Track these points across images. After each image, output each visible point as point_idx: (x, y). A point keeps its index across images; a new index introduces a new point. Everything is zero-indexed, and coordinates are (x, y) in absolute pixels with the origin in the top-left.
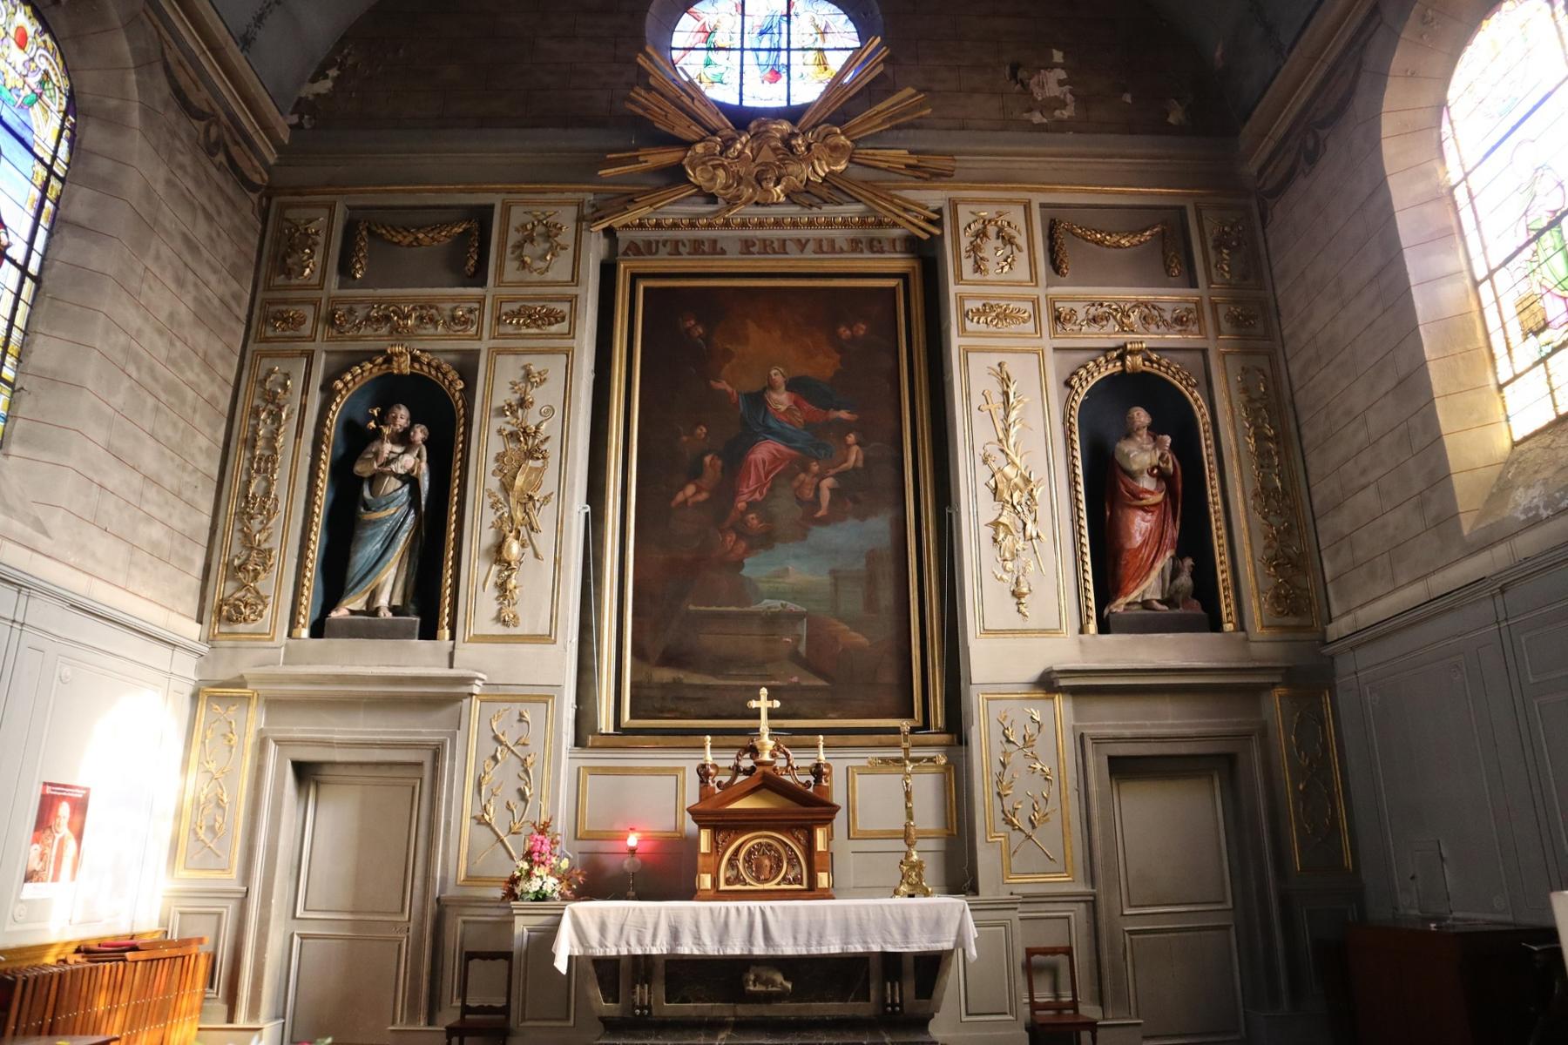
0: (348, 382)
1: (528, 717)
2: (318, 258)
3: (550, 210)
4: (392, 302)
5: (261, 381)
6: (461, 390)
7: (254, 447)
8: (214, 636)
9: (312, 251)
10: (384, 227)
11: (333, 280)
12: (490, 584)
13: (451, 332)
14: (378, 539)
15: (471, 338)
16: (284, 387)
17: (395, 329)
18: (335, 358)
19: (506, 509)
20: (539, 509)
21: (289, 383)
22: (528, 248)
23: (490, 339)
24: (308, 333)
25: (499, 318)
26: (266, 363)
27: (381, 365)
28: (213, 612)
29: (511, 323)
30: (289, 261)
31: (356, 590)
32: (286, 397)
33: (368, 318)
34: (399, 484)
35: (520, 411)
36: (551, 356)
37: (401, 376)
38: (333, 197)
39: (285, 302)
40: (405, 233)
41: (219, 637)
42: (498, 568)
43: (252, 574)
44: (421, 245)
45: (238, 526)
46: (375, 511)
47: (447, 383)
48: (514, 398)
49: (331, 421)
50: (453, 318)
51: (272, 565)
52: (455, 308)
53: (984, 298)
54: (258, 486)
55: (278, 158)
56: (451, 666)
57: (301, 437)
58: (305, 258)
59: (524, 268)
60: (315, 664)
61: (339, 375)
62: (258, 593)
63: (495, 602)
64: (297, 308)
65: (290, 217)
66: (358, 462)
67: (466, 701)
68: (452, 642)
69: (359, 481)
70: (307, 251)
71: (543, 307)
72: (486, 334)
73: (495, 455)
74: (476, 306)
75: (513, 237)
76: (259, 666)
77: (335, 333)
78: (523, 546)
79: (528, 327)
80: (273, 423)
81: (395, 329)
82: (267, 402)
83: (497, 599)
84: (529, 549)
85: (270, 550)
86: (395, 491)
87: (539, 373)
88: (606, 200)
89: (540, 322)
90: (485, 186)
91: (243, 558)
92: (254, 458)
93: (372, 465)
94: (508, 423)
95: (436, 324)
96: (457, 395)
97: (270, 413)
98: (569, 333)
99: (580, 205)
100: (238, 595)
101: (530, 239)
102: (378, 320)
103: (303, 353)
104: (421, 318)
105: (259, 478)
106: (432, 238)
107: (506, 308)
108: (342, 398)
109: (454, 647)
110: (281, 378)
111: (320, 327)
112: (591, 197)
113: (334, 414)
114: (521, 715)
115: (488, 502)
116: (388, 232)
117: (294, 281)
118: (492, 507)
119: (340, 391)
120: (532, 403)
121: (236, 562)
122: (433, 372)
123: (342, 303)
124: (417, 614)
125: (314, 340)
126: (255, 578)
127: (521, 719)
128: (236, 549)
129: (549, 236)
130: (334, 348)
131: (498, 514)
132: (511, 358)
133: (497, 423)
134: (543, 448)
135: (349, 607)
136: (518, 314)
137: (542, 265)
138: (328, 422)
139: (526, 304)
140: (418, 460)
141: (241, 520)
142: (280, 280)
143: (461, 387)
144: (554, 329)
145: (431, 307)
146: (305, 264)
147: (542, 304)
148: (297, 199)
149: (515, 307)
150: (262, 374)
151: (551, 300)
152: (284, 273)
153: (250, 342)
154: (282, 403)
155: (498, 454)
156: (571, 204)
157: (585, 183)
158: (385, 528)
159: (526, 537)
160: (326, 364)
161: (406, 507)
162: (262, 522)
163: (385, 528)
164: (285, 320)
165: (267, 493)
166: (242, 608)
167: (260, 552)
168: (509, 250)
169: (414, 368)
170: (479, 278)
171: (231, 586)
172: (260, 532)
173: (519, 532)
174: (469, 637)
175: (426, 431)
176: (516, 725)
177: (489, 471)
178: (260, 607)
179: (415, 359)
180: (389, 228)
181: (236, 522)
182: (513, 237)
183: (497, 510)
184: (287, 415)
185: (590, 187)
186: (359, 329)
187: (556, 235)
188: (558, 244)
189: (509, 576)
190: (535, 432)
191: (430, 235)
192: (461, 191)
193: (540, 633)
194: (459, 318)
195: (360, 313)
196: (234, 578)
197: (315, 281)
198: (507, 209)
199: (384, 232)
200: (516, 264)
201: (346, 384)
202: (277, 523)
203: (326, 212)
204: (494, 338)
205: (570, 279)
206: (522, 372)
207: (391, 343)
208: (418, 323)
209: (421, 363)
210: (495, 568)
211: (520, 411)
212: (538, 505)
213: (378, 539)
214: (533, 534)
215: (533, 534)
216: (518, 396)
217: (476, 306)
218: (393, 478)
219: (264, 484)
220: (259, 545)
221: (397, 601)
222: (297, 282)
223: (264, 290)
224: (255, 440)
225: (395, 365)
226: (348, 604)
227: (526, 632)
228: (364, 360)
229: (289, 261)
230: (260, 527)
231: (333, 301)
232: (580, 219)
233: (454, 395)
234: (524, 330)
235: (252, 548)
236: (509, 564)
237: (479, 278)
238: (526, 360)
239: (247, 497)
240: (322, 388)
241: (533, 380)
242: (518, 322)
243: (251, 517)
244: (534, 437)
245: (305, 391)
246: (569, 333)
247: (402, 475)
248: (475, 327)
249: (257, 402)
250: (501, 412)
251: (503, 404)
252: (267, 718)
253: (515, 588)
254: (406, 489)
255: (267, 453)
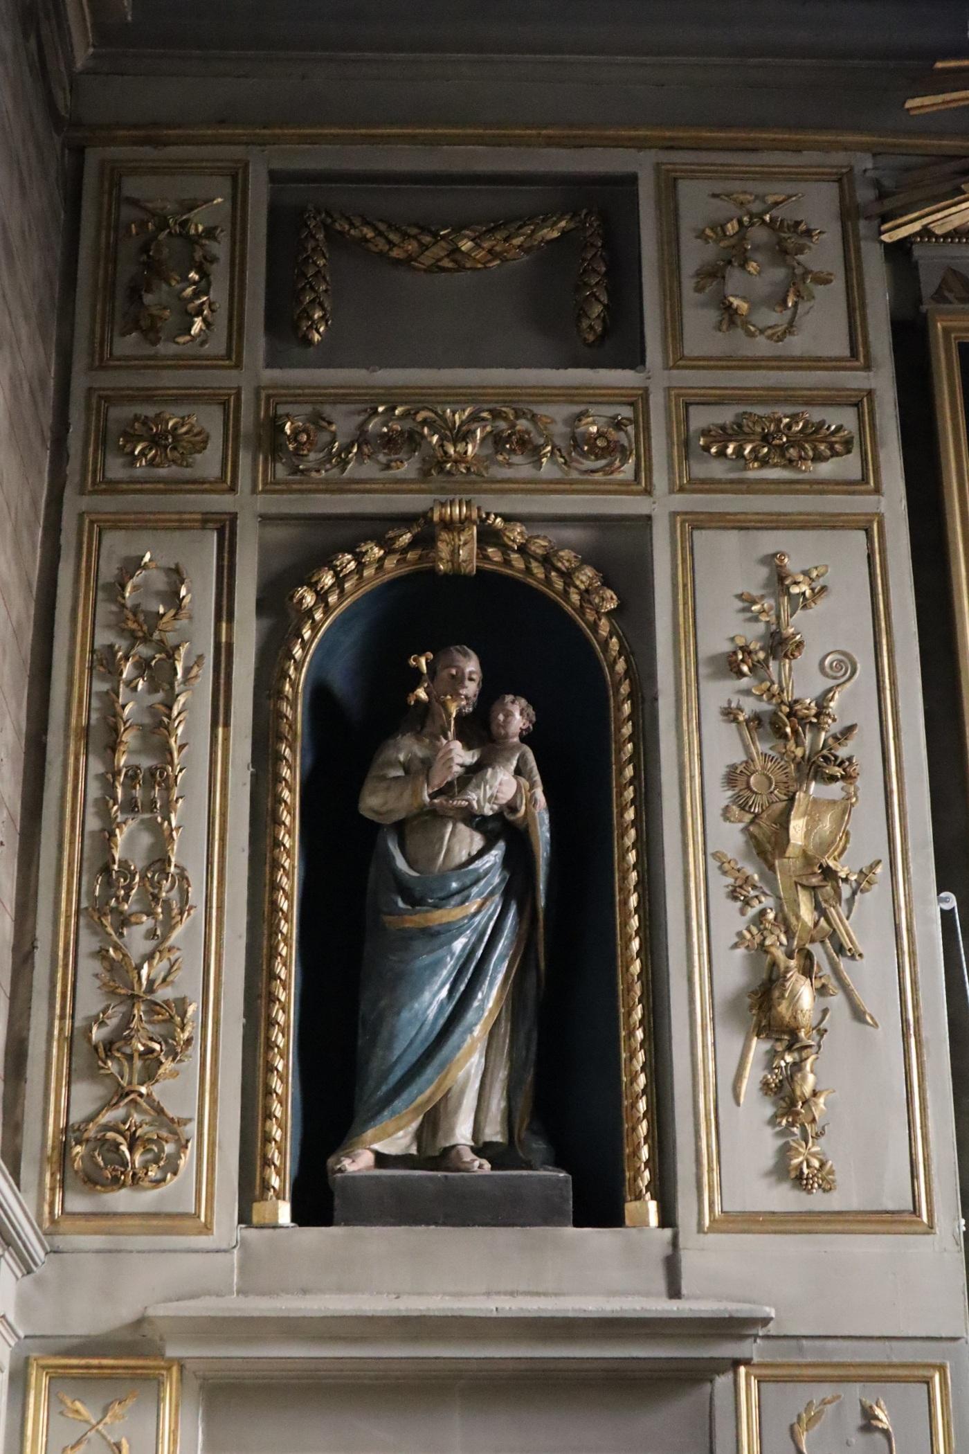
0: (327, 593)
1: (884, 1418)
2: (219, 293)
3: (775, 191)
4: (419, 398)
5: (108, 587)
6: (610, 614)
7: (113, 747)
8: (53, 1221)
9: (204, 275)
10: (366, 223)
11: (256, 342)
12: (749, 1084)
13: (575, 475)
14: (445, 972)
15: (624, 489)
16: (173, 599)
17: (435, 465)
18: (279, 533)
19: (768, 902)
20: (851, 901)
21: (183, 592)
22: (735, 278)
23: (671, 492)
24: (213, 471)
25: (686, 444)
26: (116, 545)
27: (404, 550)
28: (44, 1160)
29: (722, 454)
30: (148, 299)
31: (398, 1103)
32: (178, 624)
33: (361, 437)
34: (478, 842)
35: (773, 665)
36: (828, 534)
37: (456, 578)
38: (238, 151)
39: (147, 396)
40: (427, 239)
41: (66, 1225)
42: (767, 1046)
43: (138, 1063)
44: (461, 268)
45: (89, 943)
46: (436, 907)
47: (575, 598)
48: (752, 634)
49: (294, 685)
50: (577, 441)
51: (189, 1041)
52: (579, 417)
53: (739, 400)
54: (131, 839)
55: (94, 56)
56: (674, 1291)
57: (227, 725)
58: (189, 291)
59: (732, 323)
60: (321, 1291)
61: (304, 573)
62: (160, 1111)
63: (769, 1131)
64: (183, 411)
65: (136, 195)
66: (369, 785)
67: (722, 1381)
68: (668, 1232)
69: (370, 831)
70: (193, 275)
71: (795, 418)
72: (660, 480)
73: (723, 771)
74: (626, 412)
75: (694, 256)
76: (169, 1300)
77: (281, 471)
78: (822, 991)
79: (764, 463)
80: (153, 688)
81: (435, 465)
82: (134, 638)
83: (773, 1121)
84: (837, 1001)
85: (182, 1004)
86: (472, 859)
87: (806, 573)
88: (907, 169)
89: (793, 452)
90: (611, 133)
91: (113, 1022)
92: (116, 774)
93: (416, 793)
94: (747, 692)
95: (535, 453)
96: (604, 627)
97: (143, 666)
98: (223, 479)
99: (844, 180)
100: (107, 1117)
101: (737, 255)
102: (389, 442)
103: (206, 520)
104: (497, 441)
105: (132, 824)
106: (490, 251)
107: (701, 418)
108: (315, 628)
109: (675, 1243)
110: (160, 582)
111: (244, 459)
112: (865, 162)
113: (298, 669)
114: (868, 1415)
115: (721, 884)
116: (380, 234)
117: (164, 348)
118: (733, 895)
119: (310, 613)
120: (800, 645)
121: (97, 1034)
122: (538, 571)
123: (296, 400)
124: (559, 1164)
125: (233, 489)
126: (150, 1075)
127: (868, 1423)
128: (90, 1000)
129: (784, 252)
130: (273, 510)
131: (751, 912)
132: (731, 538)
133: (719, 693)
134: (842, 752)
135: (376, 1146)
136: (735, 432)
137: (775, 318)
138: (287, 687)
139: (749, 409)
140: (523, 781)
141: (97, 929)
142: (127, 344)
143: (612, 606)
144: (825, 469)
145: (519, 414)
146: (191, 307)
147: (790, 410)
148: (147, 152)
149: (725, 415)
150: (109, 571)
151: (810, 402)
152: (136, 326)
153: (69, 493)
154: (171, 639)
155: (733, 768)
156: (820, 177)
157: (857, 129)
158: (459, 945)
159: (827, 970)
160: (265, 552)
161: (496, 901)
162: (151, 934)
163: (459, 945)
164: (155, 441)
165: (160, 861)
166: (124, 1148)
167: (153, 1008)
168: (688, 284)
169: (486, 558)
170: (634, 358)
171: (86, 1097)
172: (149, 957)
173: (809, 956)
174: (713, 1221)
175: (531, 711)
176: (857, 1439)
177: (714, 812)
178: (169, 1148)
179: (488, 536)
180: (382, 227)
181: (84, 933)
182: (694, 256)
183: (747, 903)
184: (187, 670)
185: (866, 139)
186: (345, 463)
187: (800, 250)
188: (807, 272)
189: (797, 1066)
190: (817, 716)
191: (486, 245)
192: (550, 142)
193: (891, 1206)
194: (591, 440)
195: (343, 424)
196: (94, 1074)
197: (218, 345)
198: (668, 186)
199: (370, 234)
200: (712, 315)
201: (322, 597)
202: (192, 928)
203: (226, 184)
204: (682, 490)
205: (846, 352)
206: (763, 572)
207: (443, 498)
208: (488, 450)
209: (505, 548)
210: (758, 1047)
211: (773, 665)
212: (846, 891)
213: (445, 972)
214: (843, 963)
215: (843, 963)
216: (760, 628)
217: (626, 412)
218: (461, 827)
219: (146, 839)
220: (151, 989)
221: (494, 1133)
222: (171, 349)
223: (91, 368)
224: (115, 730)
225: (444, 550)
226: (378, 1139)
227: (854, 1204)
228: (366, 539)
229: (148, 299)
230: (148, 946)
231: (273, 397)
232: (848, 214)
233: (594, 627)
234: (755, 473)
235: (133, 998)
236: (793, 1033)
237: (634, 358)
238: (770, 541)
239: (106, 870)
240: (263, 607)
241: (795, 590)
242: (739, 452)
243: (124, 921)
244: (817, 728)
245: (225, 611)
246: (865, 480)
247: (485, 819)
248: (631, 461)
249: (104, 638)
250: (730, 666)
251: (727, 647)
252: (207, 1434)
253: (815, 1094)
254: (495, 856)
255: (146, 763)
